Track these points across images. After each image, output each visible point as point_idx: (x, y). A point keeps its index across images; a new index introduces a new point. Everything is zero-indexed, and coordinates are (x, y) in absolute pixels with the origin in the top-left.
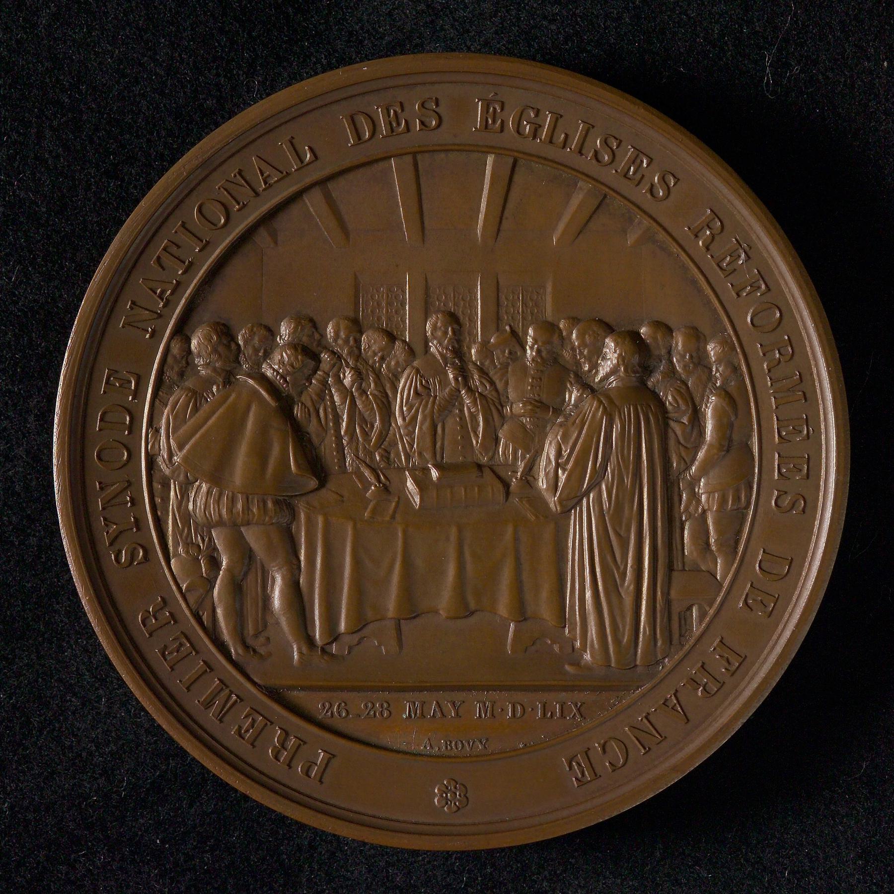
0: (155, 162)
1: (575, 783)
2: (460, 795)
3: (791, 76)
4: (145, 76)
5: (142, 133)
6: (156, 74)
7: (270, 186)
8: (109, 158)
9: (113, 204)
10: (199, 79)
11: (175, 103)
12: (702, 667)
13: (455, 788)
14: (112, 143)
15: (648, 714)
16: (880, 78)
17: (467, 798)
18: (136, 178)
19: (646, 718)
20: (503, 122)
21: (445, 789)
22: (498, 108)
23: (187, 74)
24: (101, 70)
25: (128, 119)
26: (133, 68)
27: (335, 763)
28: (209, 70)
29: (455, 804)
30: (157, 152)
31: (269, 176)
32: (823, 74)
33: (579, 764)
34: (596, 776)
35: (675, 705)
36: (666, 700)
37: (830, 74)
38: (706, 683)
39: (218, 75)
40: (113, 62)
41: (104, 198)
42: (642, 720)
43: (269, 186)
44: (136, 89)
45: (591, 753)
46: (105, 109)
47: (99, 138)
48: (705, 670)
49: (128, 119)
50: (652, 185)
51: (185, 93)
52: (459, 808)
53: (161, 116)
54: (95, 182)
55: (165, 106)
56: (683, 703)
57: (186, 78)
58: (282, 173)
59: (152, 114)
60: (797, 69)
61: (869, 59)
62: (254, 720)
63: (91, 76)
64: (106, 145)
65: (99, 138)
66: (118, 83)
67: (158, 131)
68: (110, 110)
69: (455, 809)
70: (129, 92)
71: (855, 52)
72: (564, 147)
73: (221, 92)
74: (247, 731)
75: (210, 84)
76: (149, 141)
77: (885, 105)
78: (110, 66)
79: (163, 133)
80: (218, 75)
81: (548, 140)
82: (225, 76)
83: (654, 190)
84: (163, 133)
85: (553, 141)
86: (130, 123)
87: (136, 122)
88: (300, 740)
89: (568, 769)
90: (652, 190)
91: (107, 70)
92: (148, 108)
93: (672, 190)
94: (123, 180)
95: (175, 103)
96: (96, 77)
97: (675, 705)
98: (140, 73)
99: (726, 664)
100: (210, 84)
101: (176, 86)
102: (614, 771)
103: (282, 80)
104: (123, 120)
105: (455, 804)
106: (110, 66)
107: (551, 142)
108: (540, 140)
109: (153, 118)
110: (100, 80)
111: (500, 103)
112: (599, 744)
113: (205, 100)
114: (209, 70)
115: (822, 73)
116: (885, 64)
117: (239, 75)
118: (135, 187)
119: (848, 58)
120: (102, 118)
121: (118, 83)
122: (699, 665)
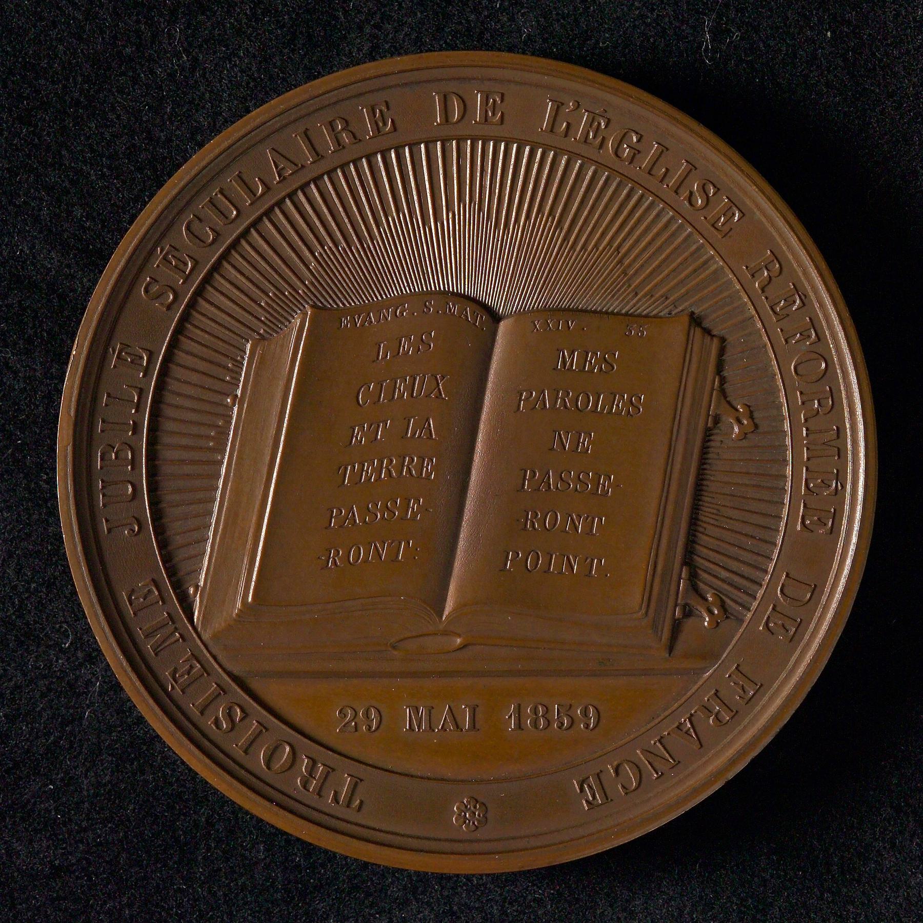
0: (70, 109)
1: (585, 805)
2: (479, 815)
3: (731, 42)
4: (63, 20)
5: (58, 78)
6: (74, 18)
7: (285, 178)
8: (23, 103)
9: (25, 151)
10: (118, 25)
11: (93, 49)
12: (716, 694)
13: (475, 807)
14: (26, 89)
15: (662, 737)
16: (823, 48)
17: (486, 818)
18: (49, 126)
19: (660, 741)
20: (604, 138)
21: (463, 808)
22: (603, 124)
23: (106, 19)
24: (17, 12)
25: (44, 64)
26: (50, 12)
27: (361, 788)
28: (130, 16)
29: (474, 823)
30: (72, 99)
31: (283, 168)
32: (764, 43)
33: (590, 787)
34: (607, 799)
35: (689, 729)
36: (681, 724)
37: (772, 43)
38: (719, 711)
39: (138, 22)
40: (31, 4)
41: (16, 145)
42: (655, 743)
43: (283, 179)
44: (53, 33)
45: (602, 776)
46: (20, 53)
47: (13, 82)
48: (718, 698)
49: (44, 64)
50: (691, 193)
51: (103, 38)
52: (477, 827)
53: (78, 62)
54: (8, 127)
55: (82, 50)
56: (697, 729)
57: (105, 23)
58: (296, 165)
59: (69, 59)
60: (737, 36)
61: (811, 29)
62: (191, 667)
63: (6, 18)
64: (20, 90)
65: (13, 82)
66: (35, 26)
67: (74, 77)
68: (26, 54)
69: (473, 828)
70: (45, 36)
71: (797, 20)
72: (566, 136)
73: (141, 39)
74: (182, 676)
75: (129, 30)
76: (65, 87)
77: (827, 77)
78: (27, 8)
79: (80, 79)
80: (138, 22)
81: (583, 140)
82: (146, 23)
83: (693, 199)
84: (80, 79)
85: (554, 131)
86: (46, 68)
87: (51, 68)
88: (329, 767)
89: (579, 791)
90: (690, 198)
91: (24, 13)
92: (65, 53)
93: (711, 199)
94: (36, 126)
95: (93, 49)
96: (13, 20)
97: (689, 729)
98: (57, 17)
99: (741, 691)
100: (129, 30)
101: (94, 32)
102: (626, 794)
103: (205, 29)
104: (39, 64)
105: (474, 823)
106: (27, 8)
107: (551, 131)
108: (575, 139)
109: (70, 63)
110: (16, 23)
111: (606, 120)
112: (612, 767)
113: (124, 46)
114: (130, 16)
115: (763, 41)
116: (829, 34)
117: (160, 23)
118: (48, 134)
119: (790, 26)
120: (17, 61)
121: (35, 26)
122: (713, 692)
